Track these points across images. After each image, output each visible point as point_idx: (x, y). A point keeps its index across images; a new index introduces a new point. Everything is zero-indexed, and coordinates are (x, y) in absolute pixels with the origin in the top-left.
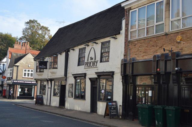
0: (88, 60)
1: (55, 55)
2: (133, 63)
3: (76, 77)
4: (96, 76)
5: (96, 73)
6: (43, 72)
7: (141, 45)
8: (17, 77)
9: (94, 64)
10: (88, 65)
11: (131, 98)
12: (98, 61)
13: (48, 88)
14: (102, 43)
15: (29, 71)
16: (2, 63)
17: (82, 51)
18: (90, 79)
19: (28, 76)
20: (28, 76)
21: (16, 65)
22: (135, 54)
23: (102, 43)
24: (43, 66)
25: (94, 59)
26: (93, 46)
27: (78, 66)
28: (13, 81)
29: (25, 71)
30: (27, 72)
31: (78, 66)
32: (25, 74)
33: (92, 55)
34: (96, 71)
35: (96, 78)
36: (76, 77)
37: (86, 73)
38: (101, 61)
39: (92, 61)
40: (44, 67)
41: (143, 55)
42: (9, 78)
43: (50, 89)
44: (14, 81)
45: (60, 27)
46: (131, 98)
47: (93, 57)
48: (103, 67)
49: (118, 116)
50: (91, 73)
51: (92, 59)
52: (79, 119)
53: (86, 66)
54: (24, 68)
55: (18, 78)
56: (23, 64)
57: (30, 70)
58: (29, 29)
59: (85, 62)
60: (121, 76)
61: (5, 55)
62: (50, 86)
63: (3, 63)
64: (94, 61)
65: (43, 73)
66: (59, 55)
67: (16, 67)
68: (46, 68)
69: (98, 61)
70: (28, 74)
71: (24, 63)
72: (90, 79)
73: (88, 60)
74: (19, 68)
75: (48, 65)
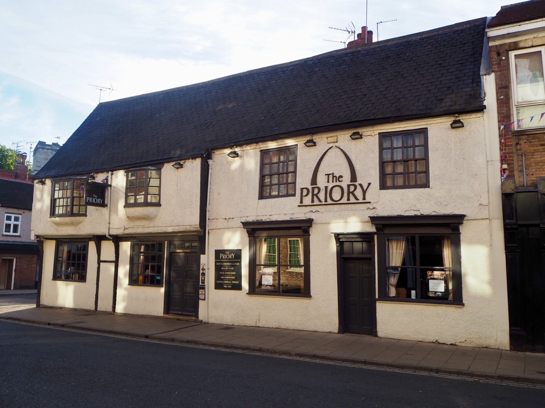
6: (85, 215)
12: (369, 184)
14: (382, 136)
19: (15, 230)
23: (382, 136)
32: (8, 226)
35: (365, 237)
40: (98, 201)
49: (280, 292)
52: (219, 346)
54: (6, 213)
61: (231, 147)
64: (349, 186)
65: (82, 218)
69: (369, 184)
73: (314, 181)
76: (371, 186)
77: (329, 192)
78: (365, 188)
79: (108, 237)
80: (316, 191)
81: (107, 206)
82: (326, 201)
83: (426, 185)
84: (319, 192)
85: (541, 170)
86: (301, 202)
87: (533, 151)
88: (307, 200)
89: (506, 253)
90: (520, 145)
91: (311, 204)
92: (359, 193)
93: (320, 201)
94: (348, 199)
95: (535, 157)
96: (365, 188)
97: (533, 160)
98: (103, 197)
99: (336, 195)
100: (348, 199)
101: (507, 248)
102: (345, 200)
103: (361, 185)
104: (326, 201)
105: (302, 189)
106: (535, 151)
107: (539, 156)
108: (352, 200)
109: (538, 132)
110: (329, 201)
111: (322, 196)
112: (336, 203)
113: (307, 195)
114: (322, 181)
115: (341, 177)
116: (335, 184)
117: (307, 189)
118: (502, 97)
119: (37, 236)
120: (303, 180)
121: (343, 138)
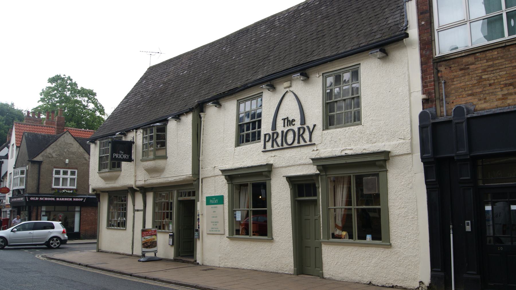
2: (434, 125)
4: (313, 170)
7: (489, 66)
8: (38, 188)
9: (301, 136)
10: (274, 140)
11: (468, 228)
12: (315, 126)
13: (135, 211)
15: (65, 173)
18: (290, 179)
22: (470, 92)
28: (29, 197)
29: (58, 173)
35: (317, 175)
36: (232, 176)
40: (125, 156)
41: (503, 93)
42: (18, 191)
43: (139, 215)
45: (152, 65)
46: (468, 228)
50: (297, 162)
51: (289, 122)
54: (55, 167)
55: (41, 191)
56: (52, 157)
57: (69, 171)
58: (54, 89)
60: (422, 163)
64: (299, 129)
67: (37, 166)
68: (130, 160)
69: (315, 126)
71: (54, 155)
72: (290, 179)
73: (274, 126)
74: (44, 166)
76: (316, 128)
77: (285, 135)
78: (311, 130)
79: (135, 188)
80: (275, 136)
81: (133, 160)
82: (282, 145)
83: (357, 119)
84: (277, 137)
85: (461, 97)
86: (265, 148)
87: (453, 77)
88: (269, 145)
89: (427, 189)
90: (441, 72)
91: (272, 149)
92: (306, 136)
93: (278, 146)
94: (299, 142)
95: (455, 83)
96: (311, 130)
97: (453, 87)
98: (130, 153)
99: (290, 138)
100: (299, 142)
101: (427, 183)
102: (296, 144)
103: (308, 127)
104: (282, 145)
105: (265, 135)
106: (455, 77)
107: (459, 82)
108: (302, 143)
109: (456, 56)
110: (285, 146)
111: (279, 140)
112: (291, 147)
113: (268, 141)
114: (280, 128)
115: (293, 120)
116: (289, 128)
117: (269, 134)
118: (423, 23)
119: (94, 190)
120: (266, 128)
121: (298, 86)
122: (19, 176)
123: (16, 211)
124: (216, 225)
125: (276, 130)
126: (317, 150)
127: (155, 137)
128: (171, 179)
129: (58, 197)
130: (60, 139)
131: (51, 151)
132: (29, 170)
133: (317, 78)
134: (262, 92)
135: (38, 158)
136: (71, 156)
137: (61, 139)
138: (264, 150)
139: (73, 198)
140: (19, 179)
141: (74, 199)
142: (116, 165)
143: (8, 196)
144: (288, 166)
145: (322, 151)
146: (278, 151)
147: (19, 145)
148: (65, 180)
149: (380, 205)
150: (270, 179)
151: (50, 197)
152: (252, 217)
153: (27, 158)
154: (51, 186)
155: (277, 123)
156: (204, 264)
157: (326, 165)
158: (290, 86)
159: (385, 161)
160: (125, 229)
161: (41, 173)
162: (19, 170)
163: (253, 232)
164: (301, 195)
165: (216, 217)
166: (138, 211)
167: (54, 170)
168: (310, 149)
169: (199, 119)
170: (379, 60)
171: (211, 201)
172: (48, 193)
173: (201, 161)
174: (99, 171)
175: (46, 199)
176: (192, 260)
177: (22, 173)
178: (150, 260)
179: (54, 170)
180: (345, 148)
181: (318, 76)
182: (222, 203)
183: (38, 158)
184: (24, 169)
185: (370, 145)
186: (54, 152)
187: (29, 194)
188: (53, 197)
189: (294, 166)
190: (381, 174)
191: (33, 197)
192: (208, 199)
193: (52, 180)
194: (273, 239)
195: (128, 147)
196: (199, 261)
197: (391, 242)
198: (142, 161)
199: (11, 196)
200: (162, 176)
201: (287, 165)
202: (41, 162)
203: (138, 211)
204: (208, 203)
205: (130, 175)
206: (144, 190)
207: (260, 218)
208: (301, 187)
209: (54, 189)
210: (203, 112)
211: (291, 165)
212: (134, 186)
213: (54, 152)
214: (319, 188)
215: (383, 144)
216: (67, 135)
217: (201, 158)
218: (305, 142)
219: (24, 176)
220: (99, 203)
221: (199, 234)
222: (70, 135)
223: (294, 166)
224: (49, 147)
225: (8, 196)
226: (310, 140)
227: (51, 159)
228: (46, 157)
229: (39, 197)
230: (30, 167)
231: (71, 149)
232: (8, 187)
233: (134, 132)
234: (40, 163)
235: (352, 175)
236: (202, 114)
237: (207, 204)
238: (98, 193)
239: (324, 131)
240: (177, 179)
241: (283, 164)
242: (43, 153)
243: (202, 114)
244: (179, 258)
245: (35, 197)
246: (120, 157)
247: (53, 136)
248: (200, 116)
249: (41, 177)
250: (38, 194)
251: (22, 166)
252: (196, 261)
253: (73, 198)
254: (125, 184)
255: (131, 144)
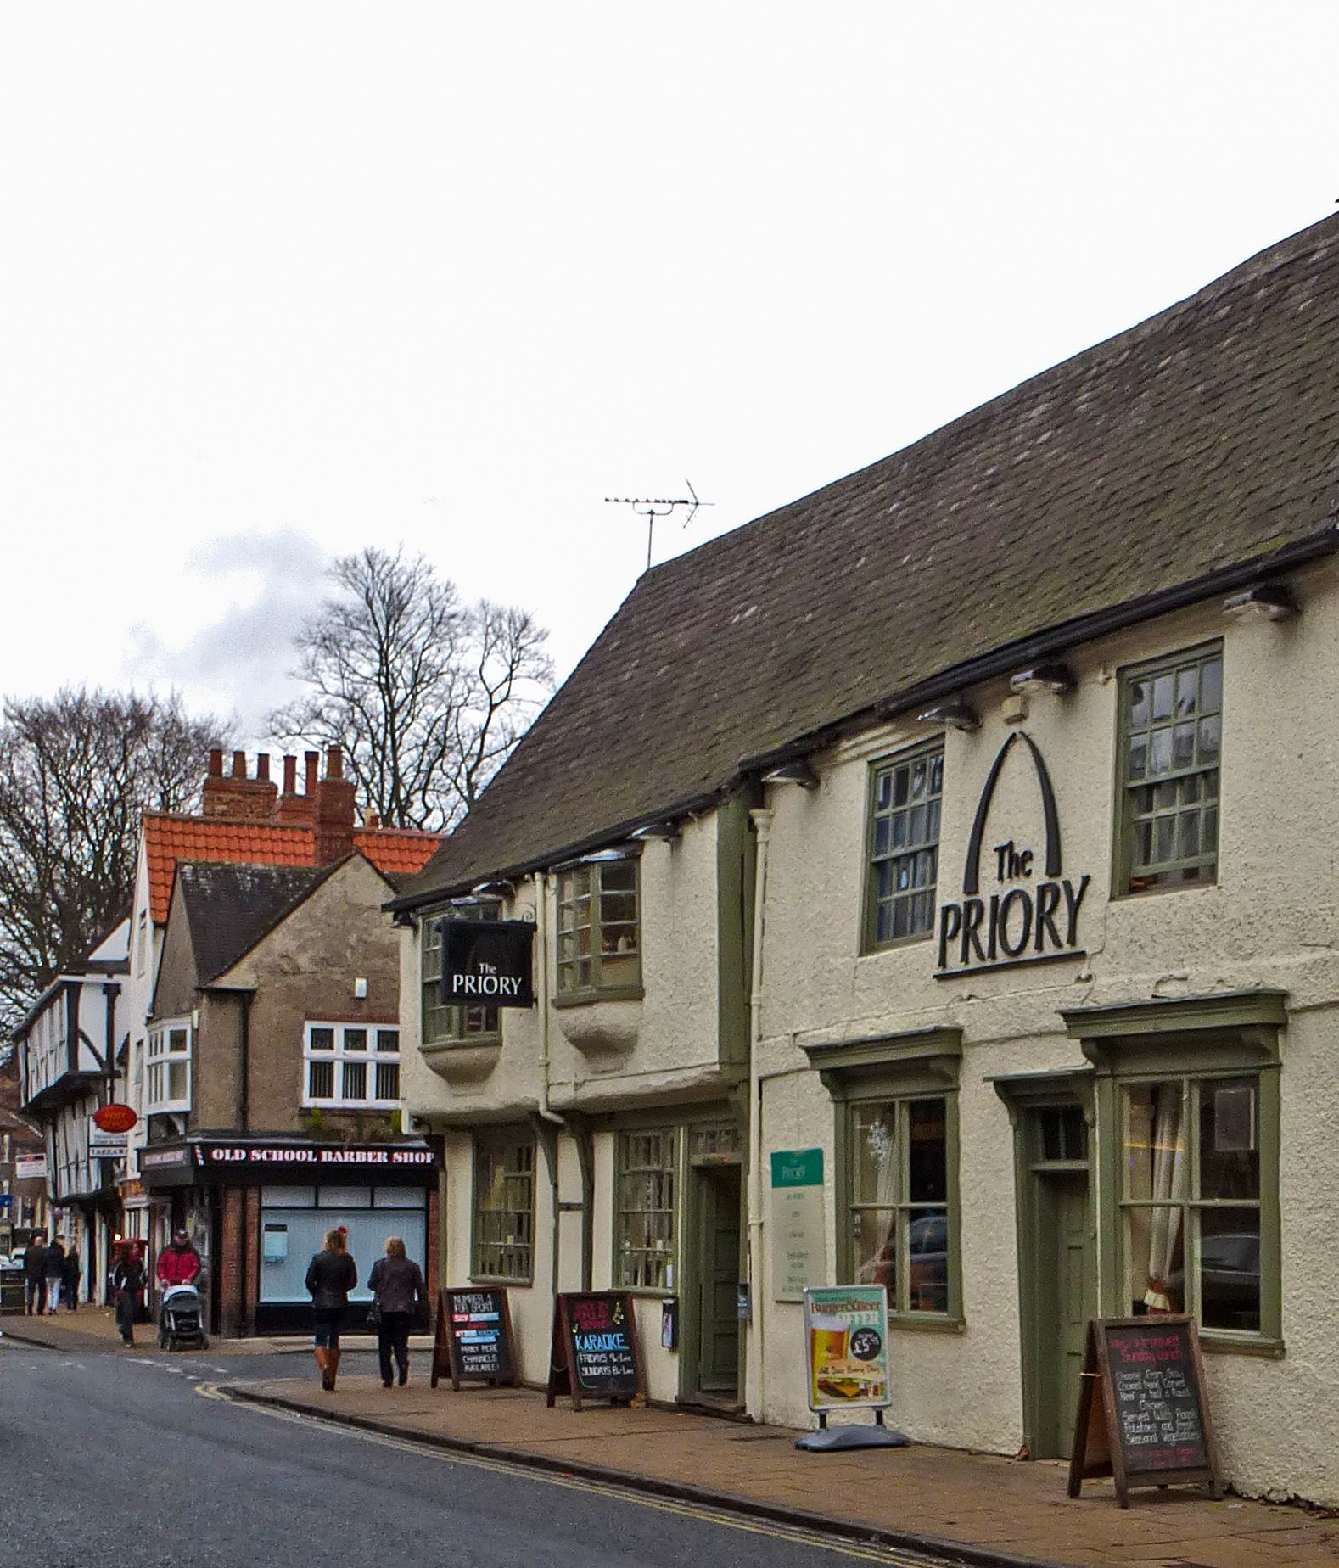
0: (971, 882)
1: (607, 854)
3: (845, 1072)
4: (1069, 1057)
5: (1074, 1018)
8: (244, 1111)
9: (1045, 918)
10: (970, 935)
12: (1086, 880)
13: (560, 1207)
15: (356, 1040)
16: (89, 978)
17: (903, 786)
19: (356, 1085)
20: (356, 1085)
21: (225, 982)
24: (486, 980)
25: (1038, 866)
26: (1028, 726)
27: (867, 948)
28: (207, 1148)
29: (322, 1039)
30: (339, 1053)
31: (867, 948)
32: (321, 1071)
33: (1018, 820)
34: (1074, 998)
36: (845, 1072)
37: (961, 1021)
38: (1129, 885)
39: (1018, 884)
40: (502, 985)
43: (572, 1223)
44: (217, 1155)
47: (1033, 839)
48: (1146, 953)
50: (1019, 1025)
51: (1015, 862)
53: (955, 948)
54: (310, 1017)
55: (255, 1123)
56: (297, 971)
57: (372, 1031)
59: (938, 906)
62: (572, 1190)
63: (103, 978)
64: (1042, 890)
66: (655, 854)
67: (232, 1012)
68: (525, 998)
69: (1086, 880)
70: (356, 1071)
71: (303, 961)
73: (971, 882)
74: (265, 1013)
75: (538, 963)
79: (549, 1115)
84: (979, 920)
86: (943, 962)
91: (961, 967)
94: (1039, 946)
100: (1039, 946)
102: (1030, 953)
103: (1067, 884)
104: (992, 955)
112: (1017, 965)
114: (991, 887)
115: (1028, 856)
122: (169, 1055)
123: (169, 1206)
124: (801, 1265)
125: (976, 892)
126: (1089, 978)
127: (597, 908)
128: (658, 1082)
129: (327, 1148)
130: (325, 888)
131: (292, 945)
132: (204, 1031)
133: (1101, 689)
134: (1221, 639)
135: (239, 978)
136: (379, 962)
137: (332, 889)
138: (939, 971)
139: (390, 1151)
140: (166, 1066)
141: (397, 1157)
142: (483, 1014)
143: (136, 1138)
144: (1010, 1039)
145: (1102, 981)
146: (980, 978)
147: (162, 919)
148: (356, 1071)
149: (1257, 1197)
150: (956, 1090)
151: (295, 1148)
152: (1197, 1242)
153: (191, 976)
154: (296, 1099)
155: (982, 863)
156: (769, 1420)
157: (1111, 1039)
158: (1021, 718)
159: (1278, 1028)
160: (530, 1286)
161: (253, 1041)
162: (169, 1026)
163: (914, 1295)
164: (1052, 1155)
165: (801, 1235)
166: (569, 1207)
167: (309, 1026)
168: (1060, 976)
169: (748, 835)
170: (1274, 625)
171: (785, 1171)
172: (282, 1128)
173: (755, 1012)
174: (424, 1041)
175: (278, 1155)
176: (730, 1406)
177: (177, 1041)
178: (849, 1445)
179: (309, 1026)
180: (1165, 974)
181: (1101, 677)
182: (816, 1178)
183: (239, 978)
184: (185, 1024)
185: (1240, 964)
186: (302, 948)
187: (210, 1133)
188: (306, 1148)
189: (1024, 1037)
190: (1265, 1078)
191: (223, 1146)
192: (779, 1159)
193: (299, 1072)
194: (963, 1322)
195: (514, 948)
196: (751, 1411)
197: (1285, 1336)
198: (562, 1005)
199: (142, 1142)
200: (630, 1068)
201: (1006, 1032)
202: (251, 993)
203: (569, 1207)
204: (778, 1181)
205: (532, 1066)
206: (584, 1121)
207: (1232, 1244)
208: (1047, 1116)
209: (306, 1112)
210: (761, 804)
211: (1014, 1033)
212: (542, 1108)
213: (302, 948)
214: (1093, 1126)
215: (1274, 961)
216: (357, 868)
217: (754, 995)
218: (1058, 944)
219: (185, 1055)
220: (441, 1174)
221: (749, 1302)
222: (368, 868)
223: (1024, 1037)
224: (282, 927)
225: (136, 1138)
226: (1072, 939)
227: (290, 980)
228: (272, 972)
229: (248, 1148)
230: (205, 1017)
231: (377, 932)
232: (131, 1105)
233: (539, 884)
234: (245, 998)
235: (1184, 1077)
236: (759, 815)
237: (774, 1185)
238: (439, 1132)
239: (1113, 904)
240: (676, 1079)
241: (994, 1028)
242: (256, 954)
243: (759, 815)
244: (699, 1398)
245: (232, 1147)
246: (483, 986)
247: (299, 876)
248: (751, 821)
249: (252, 1061)
250: (245, 1133)
251: (179, 1013)
252: (744, 1408)
253: (390, 1151)
254: (516, 1100)
255: (526, 931)
